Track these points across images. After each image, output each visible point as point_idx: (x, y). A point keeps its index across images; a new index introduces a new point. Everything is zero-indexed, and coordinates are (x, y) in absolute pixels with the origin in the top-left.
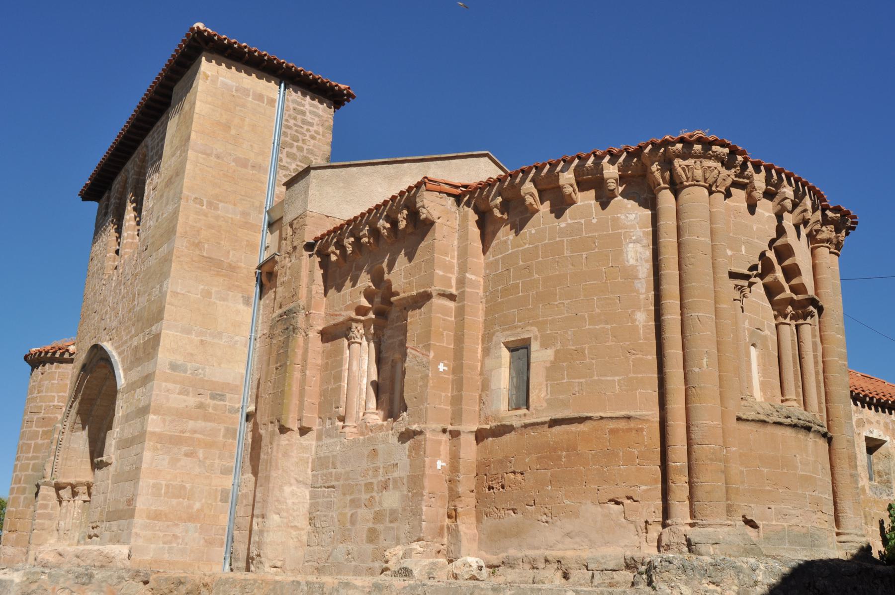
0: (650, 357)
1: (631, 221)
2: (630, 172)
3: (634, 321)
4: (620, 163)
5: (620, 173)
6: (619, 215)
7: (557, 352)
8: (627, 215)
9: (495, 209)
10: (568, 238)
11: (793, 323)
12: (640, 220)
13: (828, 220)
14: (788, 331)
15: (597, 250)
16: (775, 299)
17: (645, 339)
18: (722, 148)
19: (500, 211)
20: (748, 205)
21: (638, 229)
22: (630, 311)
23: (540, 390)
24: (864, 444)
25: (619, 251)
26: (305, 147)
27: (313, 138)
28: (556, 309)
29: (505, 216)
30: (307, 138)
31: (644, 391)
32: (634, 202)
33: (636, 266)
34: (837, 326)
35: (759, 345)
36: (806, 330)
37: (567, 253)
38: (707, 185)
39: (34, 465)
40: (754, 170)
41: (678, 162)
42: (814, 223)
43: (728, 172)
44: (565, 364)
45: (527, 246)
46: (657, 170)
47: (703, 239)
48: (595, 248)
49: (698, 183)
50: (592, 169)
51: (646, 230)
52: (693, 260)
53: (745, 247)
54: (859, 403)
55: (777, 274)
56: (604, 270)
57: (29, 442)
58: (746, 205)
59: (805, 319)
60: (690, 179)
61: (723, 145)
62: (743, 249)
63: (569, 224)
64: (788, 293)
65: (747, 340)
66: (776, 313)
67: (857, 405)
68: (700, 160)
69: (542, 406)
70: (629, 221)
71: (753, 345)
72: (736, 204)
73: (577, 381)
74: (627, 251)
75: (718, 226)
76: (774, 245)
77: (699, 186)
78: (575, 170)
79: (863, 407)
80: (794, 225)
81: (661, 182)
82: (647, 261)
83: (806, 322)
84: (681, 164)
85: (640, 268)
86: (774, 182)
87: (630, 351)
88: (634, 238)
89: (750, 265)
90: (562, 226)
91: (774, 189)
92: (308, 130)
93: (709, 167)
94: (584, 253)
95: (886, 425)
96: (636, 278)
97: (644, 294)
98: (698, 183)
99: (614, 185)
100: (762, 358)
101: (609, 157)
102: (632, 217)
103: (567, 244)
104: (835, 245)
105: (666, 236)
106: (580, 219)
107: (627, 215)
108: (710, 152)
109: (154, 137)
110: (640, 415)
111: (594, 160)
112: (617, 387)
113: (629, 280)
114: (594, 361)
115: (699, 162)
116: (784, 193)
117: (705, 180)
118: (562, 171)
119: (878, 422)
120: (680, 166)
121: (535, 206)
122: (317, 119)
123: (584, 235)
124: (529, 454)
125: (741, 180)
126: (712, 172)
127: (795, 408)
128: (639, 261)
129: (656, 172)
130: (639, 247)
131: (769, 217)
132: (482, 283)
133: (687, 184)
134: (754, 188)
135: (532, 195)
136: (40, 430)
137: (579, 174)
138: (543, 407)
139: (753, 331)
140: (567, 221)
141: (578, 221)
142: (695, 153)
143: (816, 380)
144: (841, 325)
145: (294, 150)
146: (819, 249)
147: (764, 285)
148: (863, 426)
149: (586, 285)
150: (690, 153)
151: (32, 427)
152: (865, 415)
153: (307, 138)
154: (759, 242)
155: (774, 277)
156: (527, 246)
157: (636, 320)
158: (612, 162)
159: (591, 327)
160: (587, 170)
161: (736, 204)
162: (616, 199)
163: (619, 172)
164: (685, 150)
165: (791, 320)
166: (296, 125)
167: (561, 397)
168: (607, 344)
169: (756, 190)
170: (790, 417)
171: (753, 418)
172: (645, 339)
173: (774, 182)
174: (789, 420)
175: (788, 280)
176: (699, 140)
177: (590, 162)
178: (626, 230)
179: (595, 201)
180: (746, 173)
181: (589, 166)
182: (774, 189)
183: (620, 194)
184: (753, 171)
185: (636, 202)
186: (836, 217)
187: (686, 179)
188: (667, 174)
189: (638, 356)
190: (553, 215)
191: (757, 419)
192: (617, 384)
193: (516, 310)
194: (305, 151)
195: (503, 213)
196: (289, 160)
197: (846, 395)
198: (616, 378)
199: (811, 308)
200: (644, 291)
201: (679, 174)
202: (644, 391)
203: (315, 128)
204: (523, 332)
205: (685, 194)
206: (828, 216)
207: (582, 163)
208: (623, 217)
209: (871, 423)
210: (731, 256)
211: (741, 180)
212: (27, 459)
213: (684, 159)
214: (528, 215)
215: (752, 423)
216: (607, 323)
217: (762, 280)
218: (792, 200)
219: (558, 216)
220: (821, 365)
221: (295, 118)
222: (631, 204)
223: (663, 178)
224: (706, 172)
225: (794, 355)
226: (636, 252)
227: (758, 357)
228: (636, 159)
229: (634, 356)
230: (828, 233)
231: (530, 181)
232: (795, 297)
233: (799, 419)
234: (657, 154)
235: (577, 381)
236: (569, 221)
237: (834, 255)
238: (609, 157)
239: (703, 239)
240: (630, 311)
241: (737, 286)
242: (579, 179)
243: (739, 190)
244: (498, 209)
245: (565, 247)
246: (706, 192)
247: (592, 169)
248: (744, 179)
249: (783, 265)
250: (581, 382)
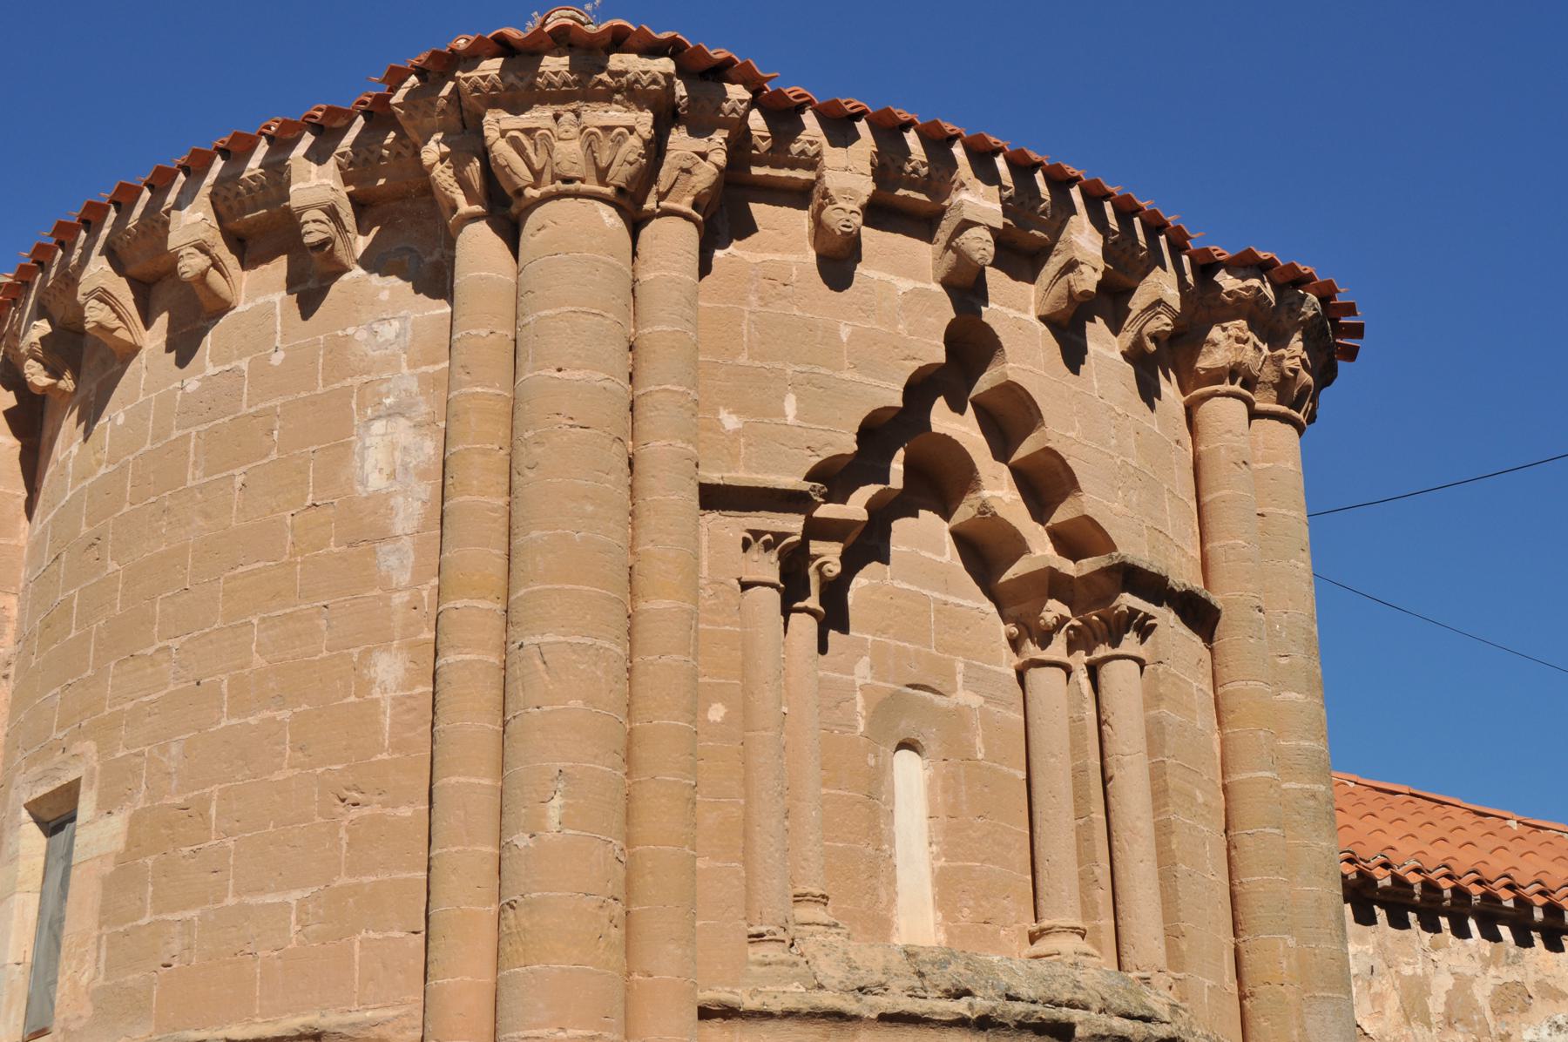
0: (405, 811)
1: (388, 344)
2: (381, 182)
3: (366, 685)
4: (342, 155)
5: (351, 188)
6: (350, 331)
7: (135, 821)
8: (375, 326)
9: (30, 362)
10: (199, 428)
11: (1080, 660)
12: (413, 340)
13: (1224, 303)
15: (274, 455)
16: (1003, 579)
17: (396, 747)
18: (643, 60)
19: (46, 367)
20: (819, 256)
21: (405, 370)
22: (355, 652)
28: (150, 670)
29: (67, 383)
31: (378, 936)
32: (401, 282)
33: (389, 495)
34: (1284, 661)
35: (932, 746)
36: (1119, 675)
37: (194, 478)
38: (609, 191)
40: (826, 134)
41: (496, 123)
42: (1144, 311)
43: (701, 144)
46: (442, 160)
47: (578, 375)
48: (270, 449)
49: (571, 187)
50: (262, 186)
51: (430, 369)
52: (538, 450)
53: (799, 400)
54: (1504, 931)
55: (986, 493)
56: (289, 520)
58: (812, 255)
59: (1115, 643)
60: (547, 177)
61: (653, 50)
62: (790, 406)
63: (209, 378)
64: (1041, 551)
65: (861, 728)
66: (1014, 630)
67: (1496, 938)
68: (574, 106)
69: (80, 1017)
70: (379, 347)
72: (768, 256)
73: (178, 916)
74: (365, 448)
75: (657, 328)
76: (972, 395)
77: (577, 195)
78: (213, 196)
79: (1524, 941)
80: (1042, 318)
81: (460, 198)
82: (423, 475)
83: (1117, 651)
84: (504, 125)
85: (400, 499)
86: (915, 170)
87: (346, 794)
88: (388, 401)
89: (816, 460)
90: (189, 389)
91: (922, 197)
93: (607, 129)
94: (237, 472)
96: (386, 536)
97: (406, 588)
98: (571, 187)
99: (323, 227)
100: (945, 791)
101: (312, 138)
102: (389, 331)
103: (196, 446)
104: (1275, 387)
105: (467, 378)
106: (240, 358)
107: (375, 326)
108: (604, 76)
110: (353, 1024)
111: (268, 154)
112: (294, 927)
113: (364, 546)
114: (230, 843)
115: (570, 116)
116: (961, 205)
117: (602, 175)
118: (178, 206)
120: (503, 133)
121: (122, 334)
123: (245, 410)
125: (784, 173)
126: (619, 144)
128: (400, 476)
129: (439, 167)
130: (402, 430)
131: (917, 293)
132: (14, 613)
133: (536, 193)
134: (825, 195)
135: (104, 297)
137: (230, 208)
138: (84, 1021)
139: (895, 696)
140: (202, 369)
141: (234, 364)
142: (550, 84)
143: (1160, 854)
144: (1303, 659)
146: (1207, 405)
147: (959, 537)
148: (1525, 1009)
149: (234, 577)
150: (532, 85)
152: (1531, 969)
154: (857, 377)
155: (977, 503)
157: (372, 682)
158: (317, 155)
159: (234, 721)
160: (250, 190)
161: (768, 256)
162: (346, 277)
163: (346, 184)
164: (511, 78)
165: (1071, 650)
167: (130, 977)
168: (278, 776)
169: (832, 202)
170: (968, 993)
171: (791, 1004)
172: (396, 747)
173: (915, 170)
174: (961, 1007)
175: (1040, 511)
176: (562, 40)
177: (254, 164)
178: (366, 378)
179: (284, 293)
180: (795, 148)
181: (253, 178)
182: (922, 197)
183: (357, 262)
184: (823, 140)
185: (405, 279)
186: (1248, 289)
187: (531, 179)
188: (474, 168)
189: (366, 811)
190: (173, 355)
191: (805, 1008)
192: (293, 917)
193: (58, 689)
195: (55, 373)
197: (1318, 900)
198: (294, 897)
199: (1127, 600)
200: (405, 578)
201: (501, 161)
202: (378, 936)
204: (65, 763)
205: (540, 226)
206: (1221, 288)
207: (231, 172)
208: (362, 335)
210: (737, 432)
211: (784, 173)
213: (516, 109)
214: (117, 367)
215: (786, 1024)
217: (946, 516)
218: (992, 230)
219: (182, 362)
222: (392, 287)
223: (464, 184)
224: (595, 146)
225: (1079, 773)
226: (393, 446)
228: (392, 134)
229: (355, 813)
230: (1230, 346)
231: (100, 254)
232: (1068, 567)
233: (1010, 998)
234: (433, 104)
235: (178, 916)
237: (1276, 423)
238: (312, 138)
239: (578, 375)
240: (355, 652)
241: (757, 534)
242: (231, 225)
243: (785, 209)
244: (37, 359)
245: (192, 458)
246: (609, 217)
247: (262, 186)
248: (792, 168)
249: (1013, 459)
250: (189, 921)
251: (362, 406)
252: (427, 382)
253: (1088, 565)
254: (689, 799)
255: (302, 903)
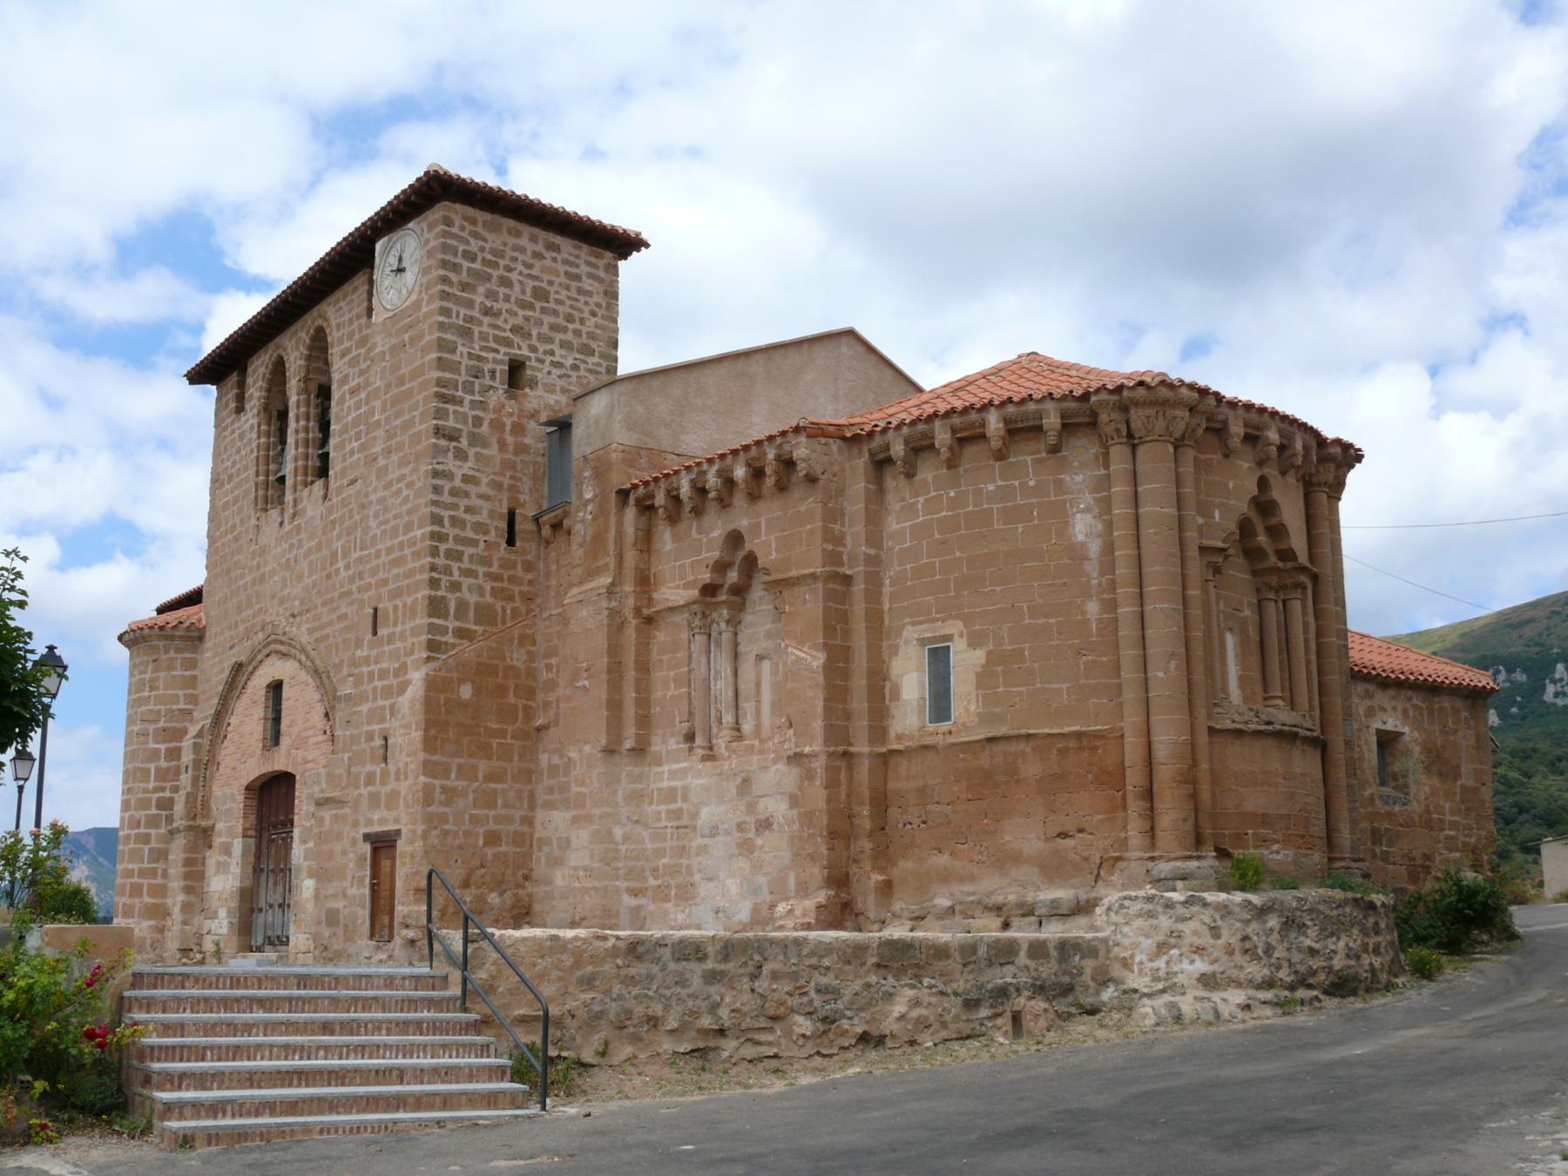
1: (1078, 483)
3: (1084, 613)
7: (989, 653)
14: (1272, 610)
15: (1036, 522)
22: (1079, 601)
23: (969, 701)
24: (1374, 739)
25: (1065, 525)
26: (584, 330)
27: (593, 314)
30: (586, 315)
39: (159, 799)
44: (1000, 669)
45: (944, 513)
57: (146, 765)
62: (1217, 514)
64: (1273, 560)
71: (1230, 629)
92: (586, 303)
95: (1405, 712)
96: (1086, 558)
109: (341, 308)
114: (1036, 665)
119: (1394, 709)
122: (596, 284)
124: (957, 781)
127: (1283, 716)
130: (1088, 517)
136: (162, 747)
145: (569, 337)
151: (147, 743)
153: (586, 315)
156: (944, 513)
166: (569, 298)
194: (584, 336)
196: (563, 352)
200: (1096, 575)
203: (595, 299)
209: (1385, 710)
212: (146, 791)
216: (1047, 616)
220: (1313, 647)
221: (568, 288)
225: (1279, 640)
227: (1235, 645)
232: (1280, 564)
236: (1000, 483)
251: (1071, 506)
252: (1098, 501)
253: (1289, 565)
254: (623, 494)
255: (1068, 689)
